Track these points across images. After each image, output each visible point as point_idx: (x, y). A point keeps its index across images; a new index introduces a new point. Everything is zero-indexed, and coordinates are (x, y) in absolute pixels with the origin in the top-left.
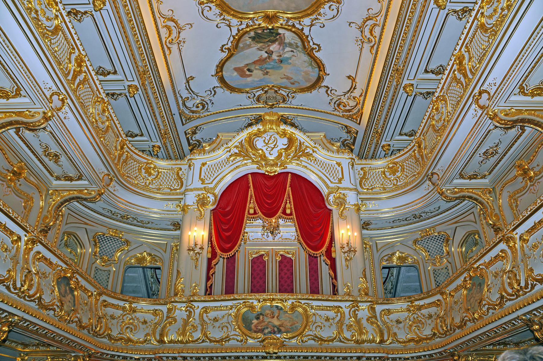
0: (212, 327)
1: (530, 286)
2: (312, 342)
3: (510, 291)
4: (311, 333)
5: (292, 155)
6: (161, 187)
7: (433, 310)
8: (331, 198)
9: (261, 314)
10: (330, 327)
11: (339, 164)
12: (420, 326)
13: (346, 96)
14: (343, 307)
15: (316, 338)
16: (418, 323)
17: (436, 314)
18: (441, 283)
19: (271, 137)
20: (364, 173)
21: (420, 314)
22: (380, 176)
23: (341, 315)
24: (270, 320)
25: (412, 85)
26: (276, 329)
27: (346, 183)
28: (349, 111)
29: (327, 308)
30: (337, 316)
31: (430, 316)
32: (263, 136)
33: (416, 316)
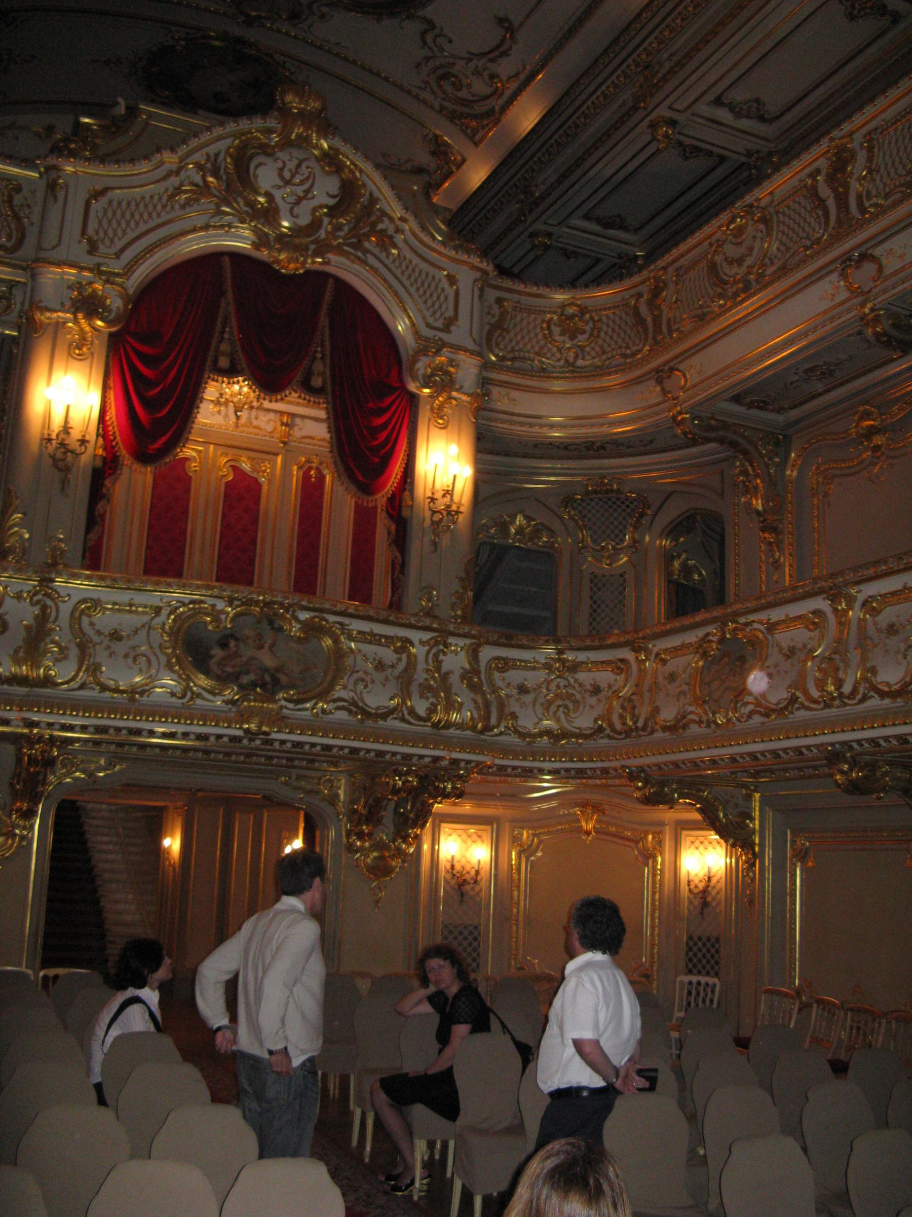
0: (107, 653)
1: (859, 696)
2: (342, 715)
3: (815, 693)
4: (343, 694)
5: (346, 229)
7: (605, 677)
8: (422, 366)
9: (232, 636)
10: (384, 685)
11: (452, 280)
12: (571, 705)
13: (472, 65)
14: (416, 642)
15: (355, 707)
16: (568, 701)
17: (610, 686)
19: (299, 166)
21: (572, 681)
22: (538, 330)
26: (267, 678)
27: (460, 334)
28: (464, 102)
30: (400, 660)
31: (596, 690)
32: (279, 154)
33: (563, 682)
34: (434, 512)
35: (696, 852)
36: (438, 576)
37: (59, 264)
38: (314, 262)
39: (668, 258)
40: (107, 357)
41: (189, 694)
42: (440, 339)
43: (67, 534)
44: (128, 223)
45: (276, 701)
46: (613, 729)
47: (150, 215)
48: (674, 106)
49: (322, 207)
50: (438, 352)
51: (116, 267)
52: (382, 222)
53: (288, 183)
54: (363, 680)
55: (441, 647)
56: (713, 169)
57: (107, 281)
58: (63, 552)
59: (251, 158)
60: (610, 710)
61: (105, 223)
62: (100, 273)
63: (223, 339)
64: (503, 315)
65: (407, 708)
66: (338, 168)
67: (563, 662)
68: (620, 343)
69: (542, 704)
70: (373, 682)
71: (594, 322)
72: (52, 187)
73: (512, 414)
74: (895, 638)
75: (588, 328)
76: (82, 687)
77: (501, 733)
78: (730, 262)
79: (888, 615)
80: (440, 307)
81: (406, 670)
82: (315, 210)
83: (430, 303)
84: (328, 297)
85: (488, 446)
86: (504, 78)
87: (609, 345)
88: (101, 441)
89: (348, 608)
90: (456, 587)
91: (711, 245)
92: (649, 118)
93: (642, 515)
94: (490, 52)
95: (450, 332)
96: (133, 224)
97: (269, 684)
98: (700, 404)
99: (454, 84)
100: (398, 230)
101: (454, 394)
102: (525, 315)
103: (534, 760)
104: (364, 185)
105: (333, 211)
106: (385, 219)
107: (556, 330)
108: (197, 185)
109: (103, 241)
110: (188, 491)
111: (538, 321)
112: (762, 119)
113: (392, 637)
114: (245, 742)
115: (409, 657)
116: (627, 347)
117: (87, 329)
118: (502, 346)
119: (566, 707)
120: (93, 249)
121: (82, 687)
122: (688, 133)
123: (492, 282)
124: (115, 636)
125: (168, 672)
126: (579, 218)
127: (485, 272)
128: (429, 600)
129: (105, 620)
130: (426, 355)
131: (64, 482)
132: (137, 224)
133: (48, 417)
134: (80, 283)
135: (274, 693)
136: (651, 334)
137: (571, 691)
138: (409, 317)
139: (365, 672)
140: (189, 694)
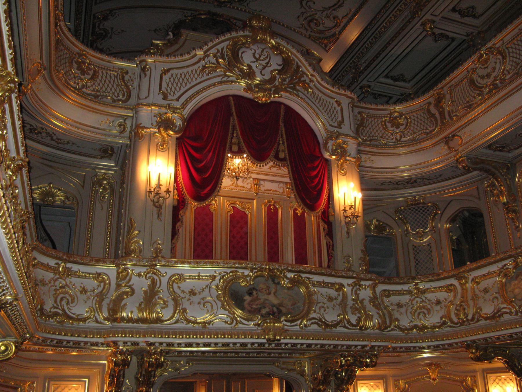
2: (315, 327)
5: (287, 80)
6: (98, 94)
7: (442, 295)
8: (331, 144)
9: (254, 288)
10: (86, 302)
11: (339, 103)
12: (426, 312)
13: (325, 13)
14: (346, 285)
15: (321, 322)
18: (421, 261)
19: (262, 51)
20: (362, 119)
21: (424, 299)
22: (380, 126)
23: (105, 285)
24: (266, 297)
25: (434, 22)
26: (275, 310)
27: (346, 129)
28: (321, 32)
29: (326, 285)
30: (339, 295)
33: (419, 300)
34: (346, 217)
35: (498, 386)
36: (351, 249)
37: (149, 105)
38: (274, 97)
39: (444, 83)
40: (176, 149)
41: (235, 322)
42: (337, 131)
43: (163, 240)
44: (181, 84)
45: (281, 322)
46: (452, 322)
47: (192, 79)
48: (433, 14)
49: (275, 70)
50: (337, 138)
51: (178, 104)
52: (303, 77)
53: (257, 60)
54: (323, 307)
55: (358, 287)
56: (449, 45)
57: (174, 112)
58: (161, 250)
59: (239, 50)
60: (449, 311)
61: (170, 85)
62: (170, 108)
63: (233, 136)
64: (363, 119)
65: (346, 320)
66: (281, 52)
67: (418, 289)
68: (422, 127)
69: (411, 313)
70: (328, 307)
71: (407, 119)
72: (143, 70)
73: (372, 168)
74: (488, 294)
75: (404, 123)
76: (176, 322)
77: (392, 330)
78: (482, 77)
79: (483, 284)
80: (335, 116)
81: (342, 300)
82: (272, 71)
83: (329, 115)
84: (282, 113)
85: (365, 185)
86: (340, 18)
87: (417, 129)
88: (176, 192)
89: (311, 270)
90: (361, 255)
91: (468, 72)
92: (421, 21)
93: (436, 214)
94: (333, 6)
95: (341, 128)
96: (184, 84)
97: (276, 313)
98: (472, 151)
99: (316, 24)
100: (311, 81)
101: (348, 158)
102: (373, 119)
103: (417, 342)
104: (294, 60)
105: (280, 72)
106: (305, 75)
107: (389, 125)
108: (214, 64)
109: (170, 93)
110: (212, 220)
111: (379, 122)
112: (474, 17)
113: (334, 283)
114: (267, 345)
115: (343, 294)
116: (427, 129)
117: (165, 136)
118: (364, 135)
119: (424, 313)
120: (165, 98)
121: (176, 322)
122: (440, 27)
123: (355, 104)
124: (192, 293)
125: (223, 310)
126: (383, 77)
127: (353, 99)
128: (349, 263)
129: (188, 285)
130: (332, 140)
131: (159, 215)
132: (186, 84)
133: (149, 181)
134: (160, 114)
135: (279, 318)
136: (439, 122)
137: (424, 304)
138: (322, 122)
139: (323, 303)
140: (235, 322)
